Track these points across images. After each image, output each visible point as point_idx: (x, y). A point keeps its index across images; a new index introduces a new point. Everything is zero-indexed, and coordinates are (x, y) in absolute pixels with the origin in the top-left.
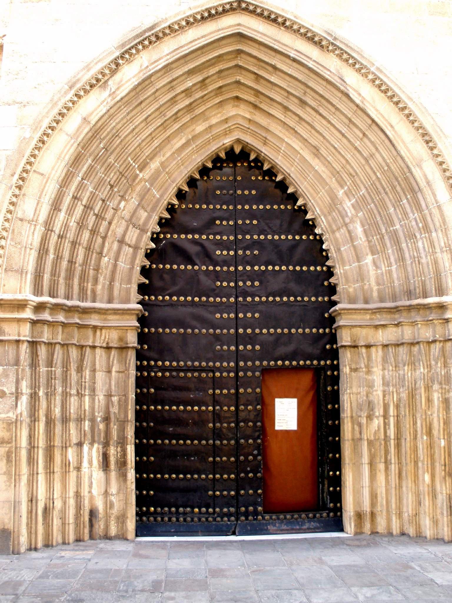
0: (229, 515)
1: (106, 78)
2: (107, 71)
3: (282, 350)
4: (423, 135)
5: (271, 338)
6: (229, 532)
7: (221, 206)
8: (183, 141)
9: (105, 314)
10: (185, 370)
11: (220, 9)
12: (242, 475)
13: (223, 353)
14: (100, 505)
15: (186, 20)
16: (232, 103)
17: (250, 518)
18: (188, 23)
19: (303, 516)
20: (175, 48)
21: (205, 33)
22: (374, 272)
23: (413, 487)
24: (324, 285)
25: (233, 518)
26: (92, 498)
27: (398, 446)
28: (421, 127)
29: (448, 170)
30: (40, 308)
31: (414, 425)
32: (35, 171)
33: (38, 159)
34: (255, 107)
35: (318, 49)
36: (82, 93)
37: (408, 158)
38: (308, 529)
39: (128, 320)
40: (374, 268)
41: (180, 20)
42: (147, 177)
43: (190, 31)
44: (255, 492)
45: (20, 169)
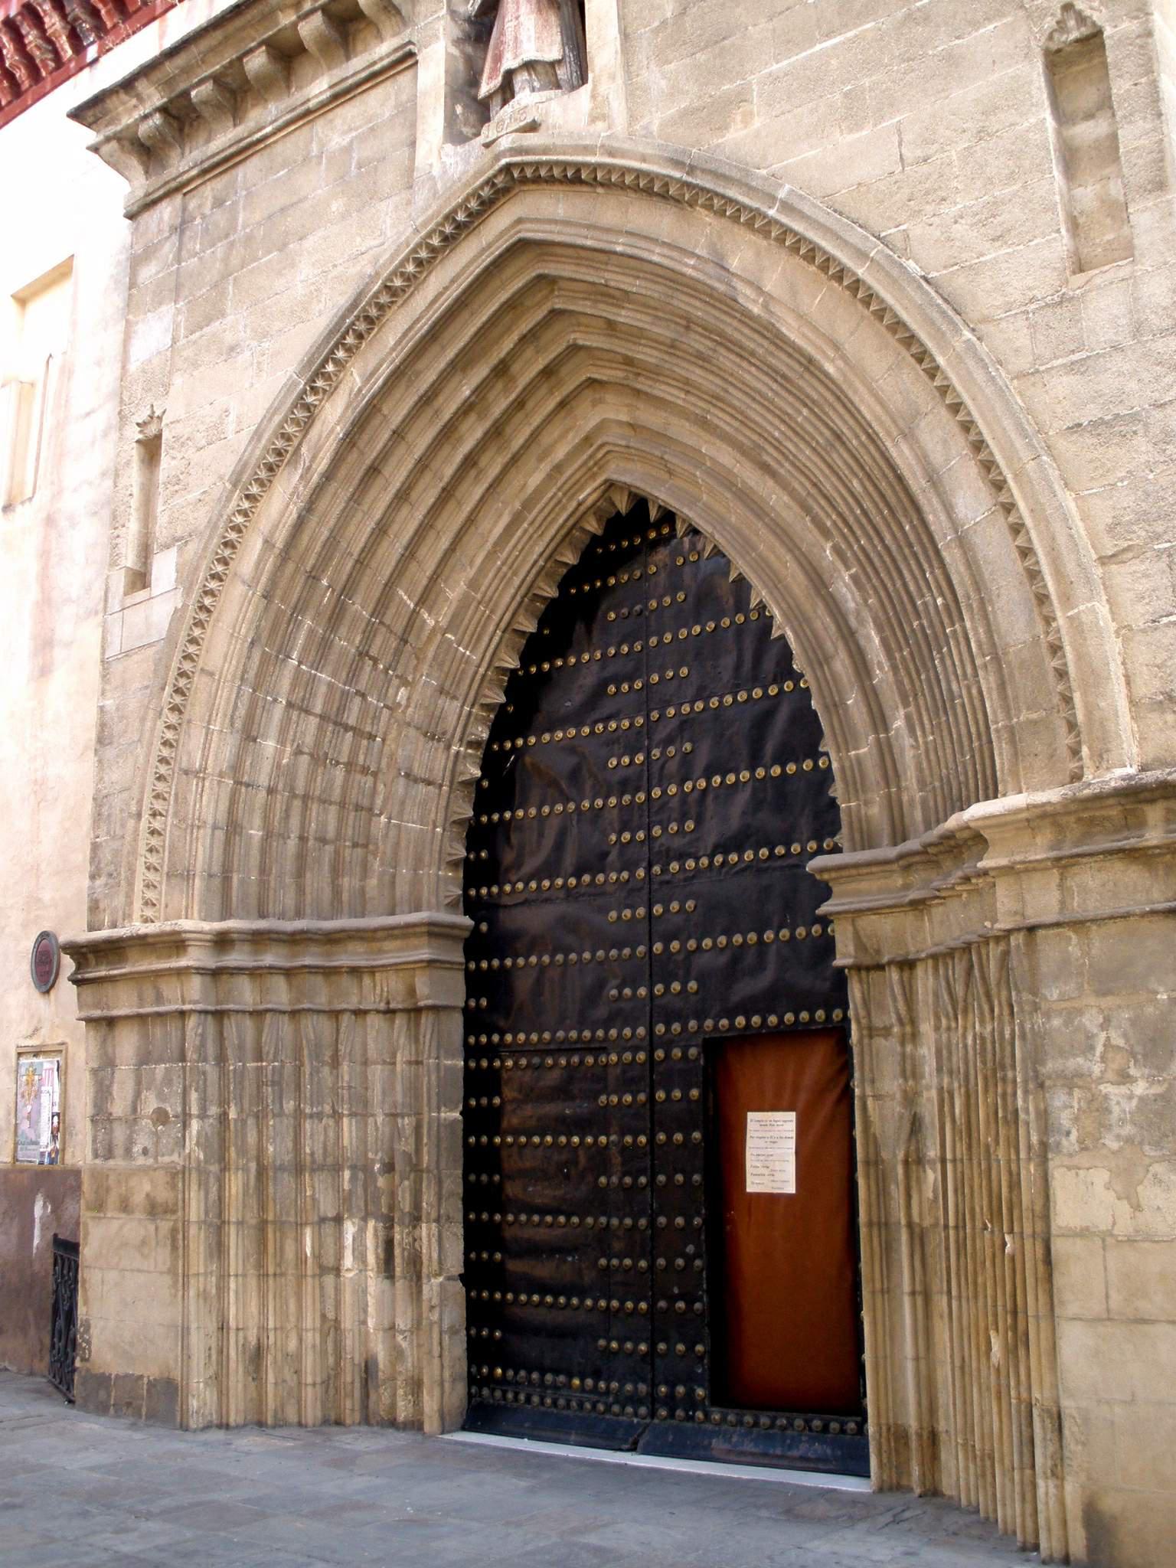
0: (635, 1400)
1: (296, 442)
2: (290, 429)
3: (746, 988)
5: (723, 960)
6: (626, 1441)
8: (505, 519)
9: (374, 940)
10: (596, 1049)
11: (473, 204)
12: (662, 1304)
13: (623, 1005)
14: (381, 1352)
15: (415, 259)
16: (589, 395)
17: (680, 1413)
19: (799, 1422)
20: (406, 327)
24: (811, 808)
25: (643, 1410)
26: (364, 1337)
30: (222, 942)
33: (204, 644)
35: (674, 209)
37: (881, 423)
38: (803, 1458)
41: (402, 264)
42: (443, 621)
43: (432, 278)
44: (690, 1348)
45: (173, 673)
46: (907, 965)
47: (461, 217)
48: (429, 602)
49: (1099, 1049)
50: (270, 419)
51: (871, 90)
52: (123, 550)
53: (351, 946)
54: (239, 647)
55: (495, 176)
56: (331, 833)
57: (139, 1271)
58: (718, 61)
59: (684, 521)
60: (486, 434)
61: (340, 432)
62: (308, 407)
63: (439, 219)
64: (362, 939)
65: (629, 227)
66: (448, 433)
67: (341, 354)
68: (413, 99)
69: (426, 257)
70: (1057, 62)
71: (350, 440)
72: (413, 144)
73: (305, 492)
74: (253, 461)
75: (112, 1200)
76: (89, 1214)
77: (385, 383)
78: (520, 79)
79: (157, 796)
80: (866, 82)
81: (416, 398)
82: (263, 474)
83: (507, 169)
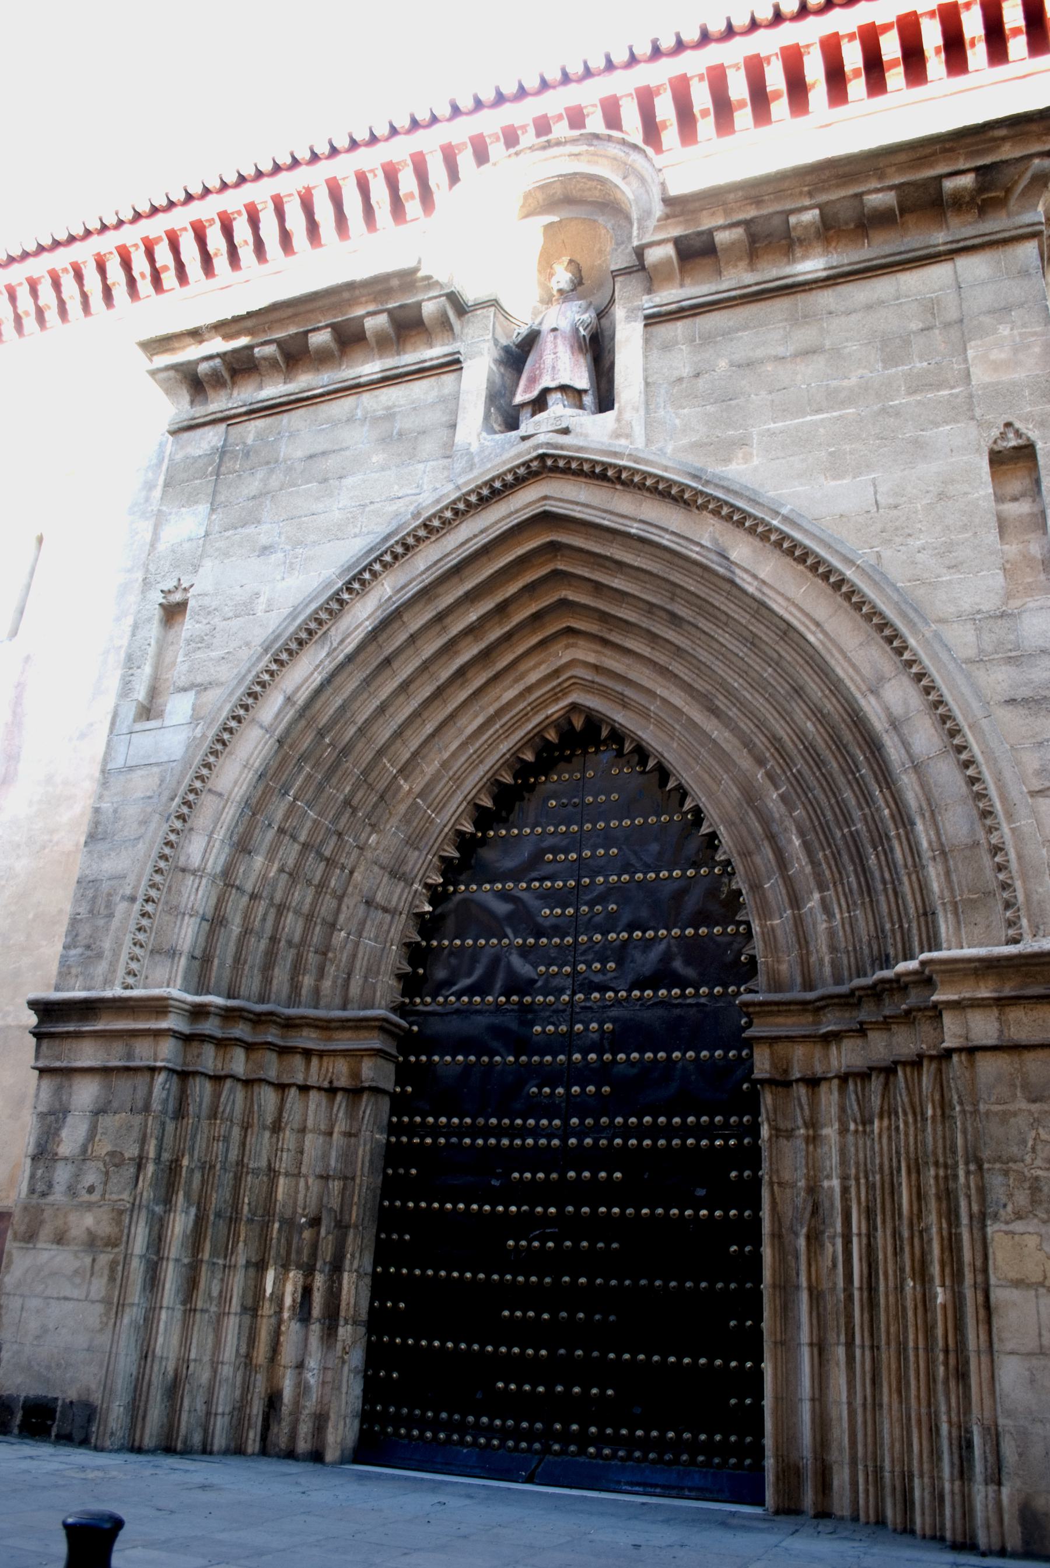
4: (881, 628)
7: (556, 828)
8: (480, 720)
11: (509, 478)
18: (456, 512)
20: (436, 558)
21: (487, 523)
22: (824, 925)
23: (895, 1405)
27: (871, 1304)
28: (875, 613)
29: (934, 688)
30: (198, 1012)
31: (895, 1254)
32: (210, 790)
33: (215, 770)
34: (605, 642)
36: (284, 656)
39: (366, 1039)
40: (824, 917)
41: (441, 511)
42: (417, 789)
43: (463, 526)
46: (813, 1082)
47: (498, 484)
48: (406, 772)
49: (1030, 1143)
50: (307, 605)
51: (851, 453)
52: (137, 687)
53: (305, 1032)
54: (249, 776)
55: (531, 461)
56: (297, 939)
57: (66, 1299)
58: (725, 415)
59: (633, 740)
60: (480, 652)
61: (369, 626)
62: (341, 602)
63: (479, 482)
64: (317, 1027)
65: (642, 517)
66: (449, 648)
67: (377, 567)
68: (456, 396)
69: (465, 508)
70: (999, 460)
71: (374, 635)
72: (454, 426)
73: (330, 666)
74: (287, 634)
75: (47, 1231)
76: (17, 1244)
77: (410, 599)
78: (554, 398)
79: (153, 886)
80: (848, 448)
81: (434, 613)
82: (294, 646)
83: (542, 457)
